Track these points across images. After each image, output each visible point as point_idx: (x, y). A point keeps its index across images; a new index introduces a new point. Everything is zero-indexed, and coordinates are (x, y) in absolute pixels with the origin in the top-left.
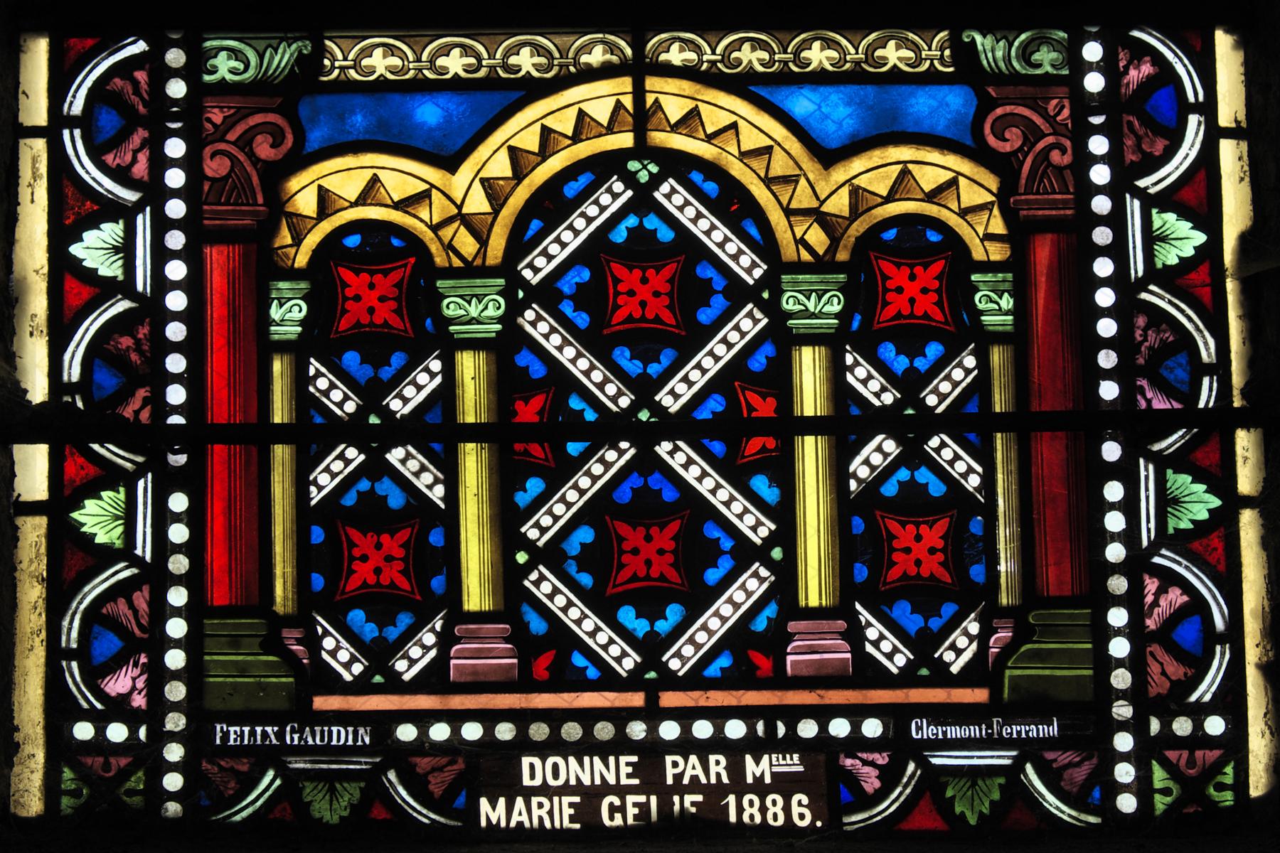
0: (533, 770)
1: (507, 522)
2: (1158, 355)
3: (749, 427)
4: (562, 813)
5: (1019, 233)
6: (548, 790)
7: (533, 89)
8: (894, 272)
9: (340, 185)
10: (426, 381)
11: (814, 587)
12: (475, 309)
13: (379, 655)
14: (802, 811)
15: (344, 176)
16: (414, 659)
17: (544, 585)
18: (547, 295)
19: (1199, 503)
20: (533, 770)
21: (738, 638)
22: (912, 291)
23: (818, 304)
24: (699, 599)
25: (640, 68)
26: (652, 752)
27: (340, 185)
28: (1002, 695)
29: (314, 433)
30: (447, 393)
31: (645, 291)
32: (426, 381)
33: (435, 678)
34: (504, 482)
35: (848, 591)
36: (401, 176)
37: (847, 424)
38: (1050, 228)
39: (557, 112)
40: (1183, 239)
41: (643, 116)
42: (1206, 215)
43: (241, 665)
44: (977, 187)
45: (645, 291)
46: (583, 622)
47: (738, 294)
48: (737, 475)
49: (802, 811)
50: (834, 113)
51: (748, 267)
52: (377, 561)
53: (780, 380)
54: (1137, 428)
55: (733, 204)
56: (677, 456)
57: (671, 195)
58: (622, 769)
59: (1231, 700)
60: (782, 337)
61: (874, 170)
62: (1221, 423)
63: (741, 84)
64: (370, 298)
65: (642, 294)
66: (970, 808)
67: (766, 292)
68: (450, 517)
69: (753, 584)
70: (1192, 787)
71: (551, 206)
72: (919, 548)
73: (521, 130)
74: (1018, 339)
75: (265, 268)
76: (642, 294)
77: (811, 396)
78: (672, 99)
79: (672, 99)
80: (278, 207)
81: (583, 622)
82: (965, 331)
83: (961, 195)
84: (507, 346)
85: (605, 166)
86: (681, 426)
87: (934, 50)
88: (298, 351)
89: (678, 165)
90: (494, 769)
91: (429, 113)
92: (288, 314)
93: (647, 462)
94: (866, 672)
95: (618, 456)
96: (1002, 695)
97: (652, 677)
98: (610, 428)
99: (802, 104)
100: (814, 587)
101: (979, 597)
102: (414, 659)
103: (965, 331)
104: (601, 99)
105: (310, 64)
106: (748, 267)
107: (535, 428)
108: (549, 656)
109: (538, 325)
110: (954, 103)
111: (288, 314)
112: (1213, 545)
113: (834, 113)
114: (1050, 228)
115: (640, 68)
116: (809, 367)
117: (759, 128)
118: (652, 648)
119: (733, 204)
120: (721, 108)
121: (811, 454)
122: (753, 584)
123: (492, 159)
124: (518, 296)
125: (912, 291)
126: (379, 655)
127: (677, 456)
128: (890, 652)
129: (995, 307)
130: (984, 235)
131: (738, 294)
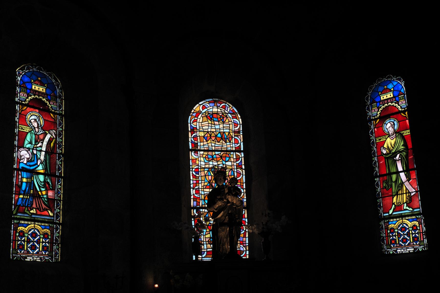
0: (28, 258)
1: (27, 246)
2: (56, 240)
3: (38, 242)
4: (29, 260)
5: (51, 234)
6: (28, 259)
7: (30, 224)
8: (45, 235)
9: (20, 228)
10: (24, 238)
11: (41, 250)
12: (26, 235)
13: (21, 252)
14: (40, 261)
15: (21, 228)
16: (22, 252)
17: (28, 249)
18: (29, 235)
19: (58, 247)
20: (28, 258)
21: (37, 252)
22: (46, 236)
23: (42, 236)
24: (35, 250)
25: (35, 224)
26: (33, 257)
27: (20, 228)
28: (48, 255)
29: (18, 241)
30: (25, 239)
31: (34, 235)
32: (24, 238)
33: (23, 253)
34: (27, 244)
35: (42, 250)
36: (23, 228)
37: (43, 242)
38: (52, 234)
39: (399, 222)
40: (58, 235)
41: (35, 226)
42: (59, 234)
43: (14, 252)
44: (49, 231)
45: (34, 235)
46: (30, 251)
47: (38, 235)
48: (38, 244)
49: (40, 261)
50: (43, 227)
51: (39, 234)
52: (21, 247)
53: (40, 240)
54: (55, 243)
55: (38, 231)
56: (35, 243)
57: (36, 230)
58: (32, 258)
59: (58, 257)
60: (409, 230)
61: (45, 230)
62: (59, 244)
63: (39, 225)
64: (21, 234)
65: (34, 235)
66: (47, 261)
67: (408, 229)
68: (24, 245)
69: (409, 241)
70: (57, 260)
71: (30, 230)
72: (45, 248)
73: (29, 226)
74: (50, 239)
75: (16, 232)
76: (34, 235)
77: (41, 241)
78: (36, 226)
79: (36, 226)
80: (17, 229)
81: (30, 251)
82: (48, 238)
83: (48, 231)
84: (28, 237)
85: (33, 229)
86: (35, 242)
87: (48, 225)
88: (18, 236)
89: (36, 229)
90: (26, 258)
91: (25, 225)
92: (17, 234)
93: (34, 243)
94: (43, 254)
95: (403, 236)
96: (48, 255)
97: (405, 246)
98: (32, 241)
99: (42, 226)
100: (41, 250)
101: (48, 251)
102: (22, 252)
103: (48, 238)
104: (33, 225)
105: (19, 222)
106: (39, 234)
107: (29, 241)
108: (28, 252)
109: (29, 236)
110: (48, 227)
111: (17, 234)
112: (58, 249)
113: (43, 227)
114: (52, 234)
115: (35, 224)
116: (41, 239)
117: (40, 227)
118: (33, 252)
119: (407, 225)
120: (38, 226)
121: (41, 243)
122: (38, 249)
123: (27, 228)
124: (28, 235)
125: (46, 236)
126: (21, 252)
127: (35, 243)
128: (415, 244)
129: (50, 237)
130: (49, 234)
131: (38, 235)
